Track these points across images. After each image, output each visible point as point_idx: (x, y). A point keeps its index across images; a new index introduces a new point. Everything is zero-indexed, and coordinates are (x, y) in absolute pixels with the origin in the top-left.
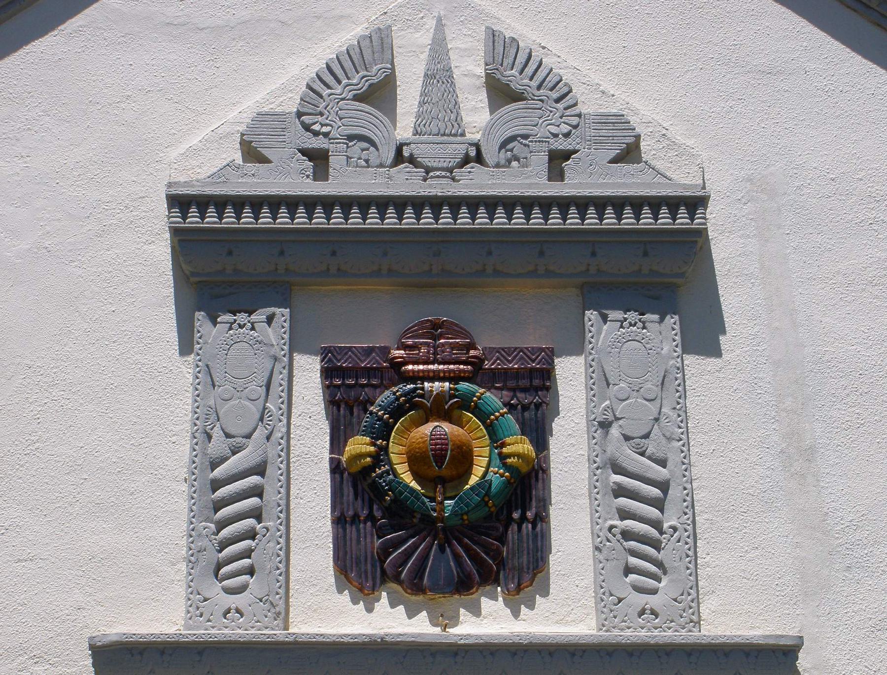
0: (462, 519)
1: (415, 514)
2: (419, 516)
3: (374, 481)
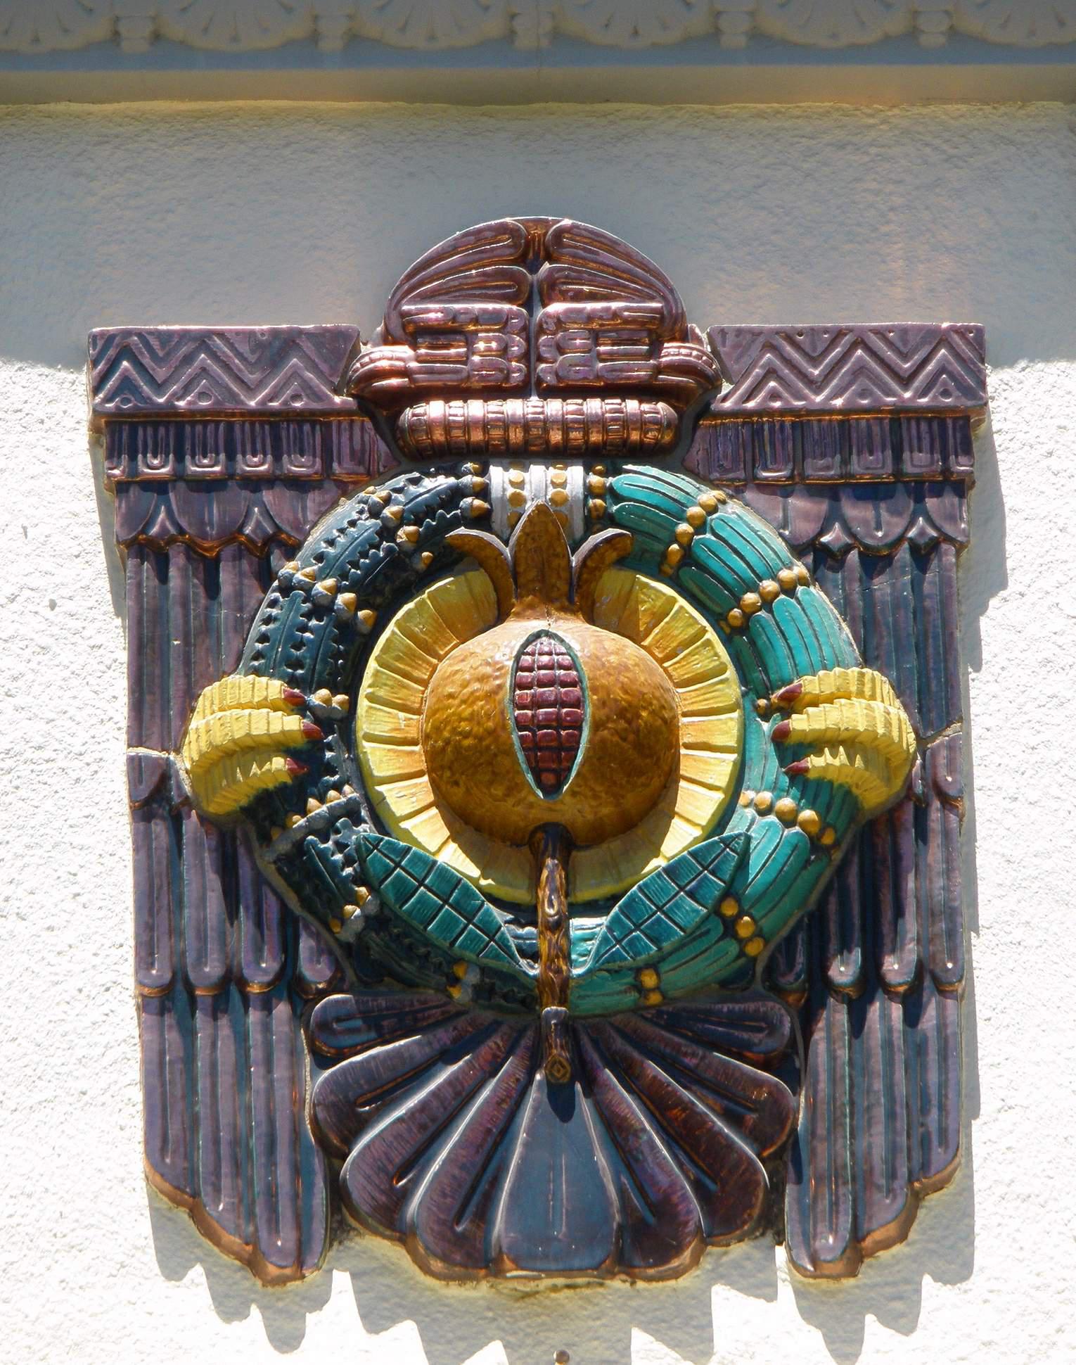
0: (639, 988)
1: (459, 971)
2: (471, 977)
3: (300, 847)
